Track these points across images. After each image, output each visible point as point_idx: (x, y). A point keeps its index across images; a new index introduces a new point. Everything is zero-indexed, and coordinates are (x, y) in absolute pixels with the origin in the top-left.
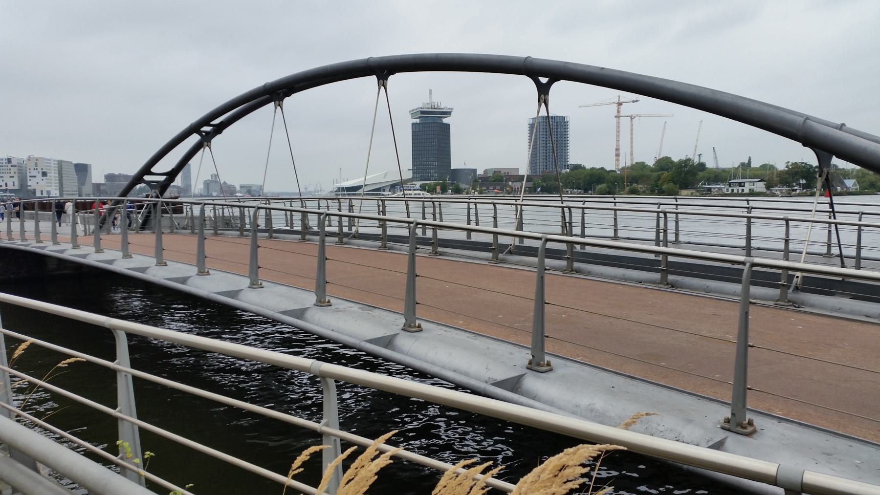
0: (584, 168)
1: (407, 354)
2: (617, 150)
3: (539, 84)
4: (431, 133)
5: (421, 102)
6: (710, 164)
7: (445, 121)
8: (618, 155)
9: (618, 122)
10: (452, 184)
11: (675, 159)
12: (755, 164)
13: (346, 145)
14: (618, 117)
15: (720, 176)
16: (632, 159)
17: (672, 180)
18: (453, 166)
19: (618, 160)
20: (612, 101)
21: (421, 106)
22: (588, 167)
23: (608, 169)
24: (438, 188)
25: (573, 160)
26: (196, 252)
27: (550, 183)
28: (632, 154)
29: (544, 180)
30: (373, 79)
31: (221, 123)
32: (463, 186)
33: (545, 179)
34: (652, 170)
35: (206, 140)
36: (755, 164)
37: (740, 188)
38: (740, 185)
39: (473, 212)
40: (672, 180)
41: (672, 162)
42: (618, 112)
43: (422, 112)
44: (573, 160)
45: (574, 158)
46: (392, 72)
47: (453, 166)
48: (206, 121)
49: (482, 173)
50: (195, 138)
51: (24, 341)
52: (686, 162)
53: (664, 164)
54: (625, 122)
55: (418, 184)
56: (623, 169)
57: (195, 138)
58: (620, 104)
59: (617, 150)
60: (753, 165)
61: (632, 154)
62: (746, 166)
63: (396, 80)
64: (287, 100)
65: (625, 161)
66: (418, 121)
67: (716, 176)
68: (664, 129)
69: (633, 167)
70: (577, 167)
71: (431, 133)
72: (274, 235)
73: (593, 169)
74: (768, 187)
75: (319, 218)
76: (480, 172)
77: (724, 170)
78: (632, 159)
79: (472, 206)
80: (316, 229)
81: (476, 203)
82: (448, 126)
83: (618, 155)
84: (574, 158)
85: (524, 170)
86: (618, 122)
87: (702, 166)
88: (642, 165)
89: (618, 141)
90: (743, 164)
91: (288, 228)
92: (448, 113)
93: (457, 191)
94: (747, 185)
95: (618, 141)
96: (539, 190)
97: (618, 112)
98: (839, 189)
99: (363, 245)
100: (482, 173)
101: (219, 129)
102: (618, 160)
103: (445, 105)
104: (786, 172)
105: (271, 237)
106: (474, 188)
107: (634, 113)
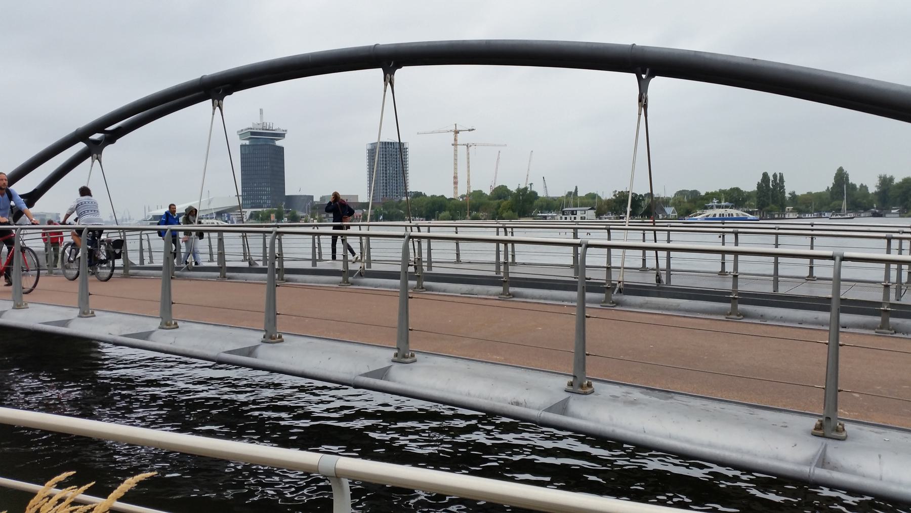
0: (425, 195)
1: (854, 473)
2: (455, 177)
3: (639, 78)
4: (263, 157)
5: (251, 121)
6: (541, 194)
7: (278, 143)
8: (456, 183)
9: (456, 150)
10: (288, 212)
11: (513, 188)
12: (581, 194)
13: (181, 167)
14: (455, 145)
15: (552, 206)
16: (469, 187)
17: (512, 208)
18: (288, 192)
19: (456, 188)
20: (449, 129)
21: (251, 126)
22: (429, 194)
23: (448, 197)
24: (273, 216)
25: (412, 187)
26: (263, 308)
27: (392, 211)
28: (468, 182)
29: (385, 208)
30: (379, 72)
31: (119, 128)
32: (300, 214)
33: (386, 206)
34: (490, 198)
35: (94, 150)
36: (581, 194)
37: (573, 217)
38: (573, 213)
39: (316, 241)
40: (512, 208)
41: (508, 191)
42: (455, 140)
43: (253, 133)
44: (412, 187)
45: (413, 186)
46: (399, 66)
47: (288, 192)
48: (99, 126)
49: (318, 200)
50: (80, 146)
51: (121, 500)
52: (835, 178)
53: (501, 193)
54: (462, 150)
55: (248, 212)
56: (462, 197)
57: (80, 146)
58: (457, 132)
59: (455, 177)
60: (579, 195)
61: (468, 182)
62: (573, 195)
63: (403, 74)
64: (227, 99)
65: (462, 191)
66: (247, 142)
67: (548, 205)
68: (498, 159)
69: (470, 195)
70: (418, 195)
71: (263, 157)
72: (228, 274)
73: (433, 196)
74: (598, 215)
75: (576, 253)
76: (317, 199)
77: (554, 199)
78: (469, 187)
79: (144, 237)
80: (260, 264)
81: (512, 228)
82: (281, 149)
83: (456, 183)
84: (413, 186)
85: (363, 196)
86: (456, 150)
87: (534, 195)
88: (479, 194)
89: (456, 169)
90: (570, 193)
91: (215, 264)
92: (281, 136)
93: (294, 219)
94: (578, 213)
95: (456, 169)
96: (381, 217)
97: (455, 140)
98: (660, 216)
99: (380, 286)
100: (318, 200)
101: (112, 137)
102: (456, 188)
103: (277, 125)
104: (614, 201)
105: (51, 273)
106: (313, 216)
107: (470, 142)
